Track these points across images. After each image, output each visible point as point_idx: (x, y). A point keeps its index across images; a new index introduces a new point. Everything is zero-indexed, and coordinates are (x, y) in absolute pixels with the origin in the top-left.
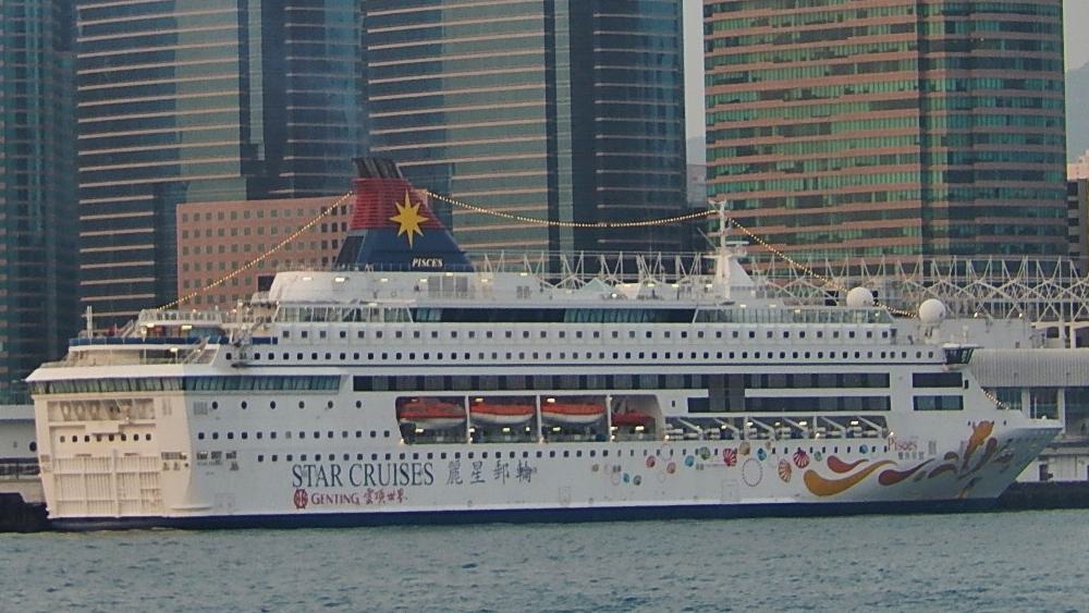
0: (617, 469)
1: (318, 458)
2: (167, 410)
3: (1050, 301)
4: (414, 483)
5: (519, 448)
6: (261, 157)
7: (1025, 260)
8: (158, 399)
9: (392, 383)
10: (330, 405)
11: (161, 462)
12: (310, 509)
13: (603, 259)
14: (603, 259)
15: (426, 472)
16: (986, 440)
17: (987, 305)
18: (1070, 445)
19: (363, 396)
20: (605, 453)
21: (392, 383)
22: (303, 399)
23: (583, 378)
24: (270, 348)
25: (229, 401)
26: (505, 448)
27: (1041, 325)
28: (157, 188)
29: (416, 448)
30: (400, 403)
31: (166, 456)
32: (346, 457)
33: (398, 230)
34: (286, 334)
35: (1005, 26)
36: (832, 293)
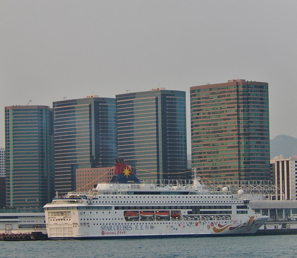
0: (172, 227)
1: (107, 224)
2: (74, 214)
3: (266, 190)
4: (128, 230)
5: (151, 222)
6: (95, 158)
7: (261, 181)
8: (72, 211)
9: (123, 208)
10: (110, 213)
11: (73, 225)
12: (105, 235)
13: (169, 181)
14: (169, 181)
15: (130, 227)
16: (253, 220)
17: (253, 191)
18: (271, 221)
19: (117, 211)
20: (170, 223)
21: (123, 208)
22: (85, 211)
23: (165, 207)
24: (96, 200)
25: (87, 212)
26: (147, 222)
27: (264, 195)
28: (72, 165)
29: (128, 222)
30: (125, 212)
31: (74, 224)
32: (113, 224)
33: (124, 174)
34: (100, 197)
35: (257, 130)
36: (219, 188)
